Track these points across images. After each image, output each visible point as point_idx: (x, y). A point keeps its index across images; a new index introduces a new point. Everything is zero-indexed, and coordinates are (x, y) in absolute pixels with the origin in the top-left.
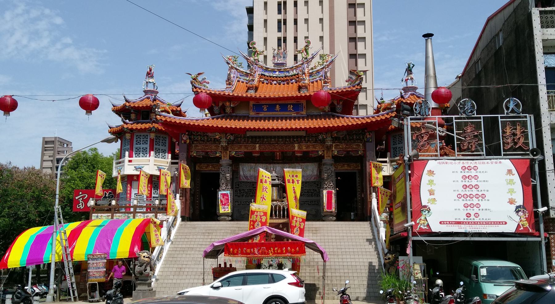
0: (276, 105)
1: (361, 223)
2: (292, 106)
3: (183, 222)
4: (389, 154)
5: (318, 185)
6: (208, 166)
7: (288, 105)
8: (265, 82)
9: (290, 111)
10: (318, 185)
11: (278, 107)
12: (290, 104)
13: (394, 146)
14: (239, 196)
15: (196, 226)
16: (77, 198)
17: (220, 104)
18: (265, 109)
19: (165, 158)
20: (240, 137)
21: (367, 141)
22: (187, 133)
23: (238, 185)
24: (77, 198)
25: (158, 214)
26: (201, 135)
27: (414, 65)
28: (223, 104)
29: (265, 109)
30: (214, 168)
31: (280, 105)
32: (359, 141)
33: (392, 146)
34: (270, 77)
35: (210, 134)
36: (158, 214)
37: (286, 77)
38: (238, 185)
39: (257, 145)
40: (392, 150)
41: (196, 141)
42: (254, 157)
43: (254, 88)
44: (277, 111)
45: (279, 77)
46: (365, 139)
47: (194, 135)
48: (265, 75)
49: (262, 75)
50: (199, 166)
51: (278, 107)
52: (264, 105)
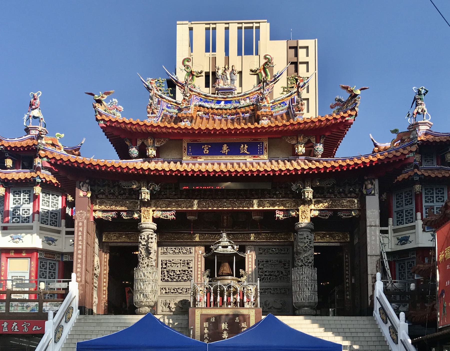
0: (221, 145)
1: (358, 318)
2: (246, 147)
3: (82, 316)
4: (390, 220)
5: (284, 264)
6: (120, 236)
7: (240, 144)
8: (205, 117)
9: (244, 154)
10: (284, 264)
11: (225, 147)
12: (244, 144)
13: (398, 209)
14: (167, 281)
15: (102, 321)
16: (22, 325)
17: (139, 143)
18: (206, 151)
19: (56, 226)
20: (170, 189)
21: (367, 195)
22: (87, 181)
23: (166, 264)
24: (22, 325)
25: (44, 304)
26: (109, 186)
27: (427, 92)
28: (143, 143)
29: (206, 151)
30: (129, 238)
31: (228, 144)
32: (353, 195)
33: (395, 209)
34: (212, 109)
35: (123, 184)
36: (44, 304)
37: (235, 108)
38: (166, 264)
39: (196, 202)
40: (395, 215)
41: (103, 193)
42: (189, 221)
43: (203, 74)
44: (224, 154)
45: (226, 109)
46: (365, 192)
47: (99, 185)
48: (204, 107)
49: (200, 106)
50: (107, 237)
51: (225, 147)
52: (204, 144)
